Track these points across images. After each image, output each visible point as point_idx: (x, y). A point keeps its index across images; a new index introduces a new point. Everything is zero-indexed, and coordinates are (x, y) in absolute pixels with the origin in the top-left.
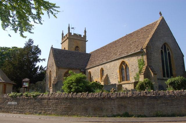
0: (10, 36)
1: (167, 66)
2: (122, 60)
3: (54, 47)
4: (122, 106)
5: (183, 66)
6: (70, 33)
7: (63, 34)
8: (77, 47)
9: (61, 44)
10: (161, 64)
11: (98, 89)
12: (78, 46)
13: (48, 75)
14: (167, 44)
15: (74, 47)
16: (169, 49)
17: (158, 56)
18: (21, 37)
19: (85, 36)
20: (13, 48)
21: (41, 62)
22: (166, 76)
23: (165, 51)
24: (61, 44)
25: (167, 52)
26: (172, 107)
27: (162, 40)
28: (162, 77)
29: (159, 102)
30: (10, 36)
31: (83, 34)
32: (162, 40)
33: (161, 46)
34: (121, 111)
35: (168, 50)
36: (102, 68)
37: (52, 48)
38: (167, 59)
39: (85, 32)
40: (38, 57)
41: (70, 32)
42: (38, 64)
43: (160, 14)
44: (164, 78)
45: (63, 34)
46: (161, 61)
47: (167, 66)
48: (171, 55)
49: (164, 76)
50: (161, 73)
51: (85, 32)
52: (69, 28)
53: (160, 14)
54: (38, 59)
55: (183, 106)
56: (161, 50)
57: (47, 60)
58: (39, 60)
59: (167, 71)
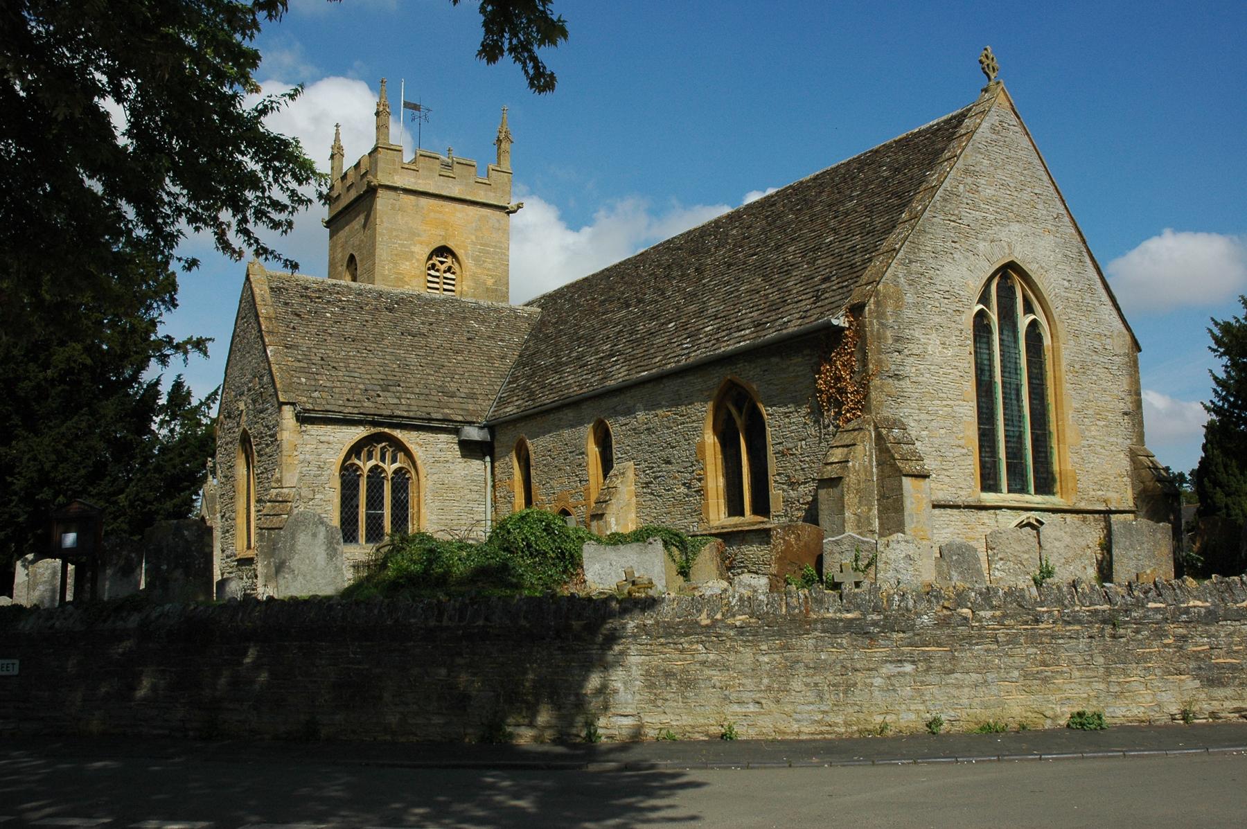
1: (1013, 420)
2: (727, 374)
4: (668, 674)
8: (443, 251)
10: (968, 410)
11: (116, 679)
13: (641, 801)
21: (176, 360)
22: (1032, 491)
23: (1008, 316)
25: (1024, 322)
27: (982, 246)
28: (971, 490)
29: (880, 652)
32: (982, 246)
33: (976, 285)
34: (659, 703)
35: (1029, 309)
38: (1017, 370)
40: (153, 324)
42: (209, 423)
44: (989, 498)
46: (970, 387)
47: (1013, 420)
48: (1047, 341)
49: (989, 482)
50: (972, 464)
54: (153, 337)
55: (1016, 673)
57: (219, 351)
58: (163, 349)
59: (1015, 454)
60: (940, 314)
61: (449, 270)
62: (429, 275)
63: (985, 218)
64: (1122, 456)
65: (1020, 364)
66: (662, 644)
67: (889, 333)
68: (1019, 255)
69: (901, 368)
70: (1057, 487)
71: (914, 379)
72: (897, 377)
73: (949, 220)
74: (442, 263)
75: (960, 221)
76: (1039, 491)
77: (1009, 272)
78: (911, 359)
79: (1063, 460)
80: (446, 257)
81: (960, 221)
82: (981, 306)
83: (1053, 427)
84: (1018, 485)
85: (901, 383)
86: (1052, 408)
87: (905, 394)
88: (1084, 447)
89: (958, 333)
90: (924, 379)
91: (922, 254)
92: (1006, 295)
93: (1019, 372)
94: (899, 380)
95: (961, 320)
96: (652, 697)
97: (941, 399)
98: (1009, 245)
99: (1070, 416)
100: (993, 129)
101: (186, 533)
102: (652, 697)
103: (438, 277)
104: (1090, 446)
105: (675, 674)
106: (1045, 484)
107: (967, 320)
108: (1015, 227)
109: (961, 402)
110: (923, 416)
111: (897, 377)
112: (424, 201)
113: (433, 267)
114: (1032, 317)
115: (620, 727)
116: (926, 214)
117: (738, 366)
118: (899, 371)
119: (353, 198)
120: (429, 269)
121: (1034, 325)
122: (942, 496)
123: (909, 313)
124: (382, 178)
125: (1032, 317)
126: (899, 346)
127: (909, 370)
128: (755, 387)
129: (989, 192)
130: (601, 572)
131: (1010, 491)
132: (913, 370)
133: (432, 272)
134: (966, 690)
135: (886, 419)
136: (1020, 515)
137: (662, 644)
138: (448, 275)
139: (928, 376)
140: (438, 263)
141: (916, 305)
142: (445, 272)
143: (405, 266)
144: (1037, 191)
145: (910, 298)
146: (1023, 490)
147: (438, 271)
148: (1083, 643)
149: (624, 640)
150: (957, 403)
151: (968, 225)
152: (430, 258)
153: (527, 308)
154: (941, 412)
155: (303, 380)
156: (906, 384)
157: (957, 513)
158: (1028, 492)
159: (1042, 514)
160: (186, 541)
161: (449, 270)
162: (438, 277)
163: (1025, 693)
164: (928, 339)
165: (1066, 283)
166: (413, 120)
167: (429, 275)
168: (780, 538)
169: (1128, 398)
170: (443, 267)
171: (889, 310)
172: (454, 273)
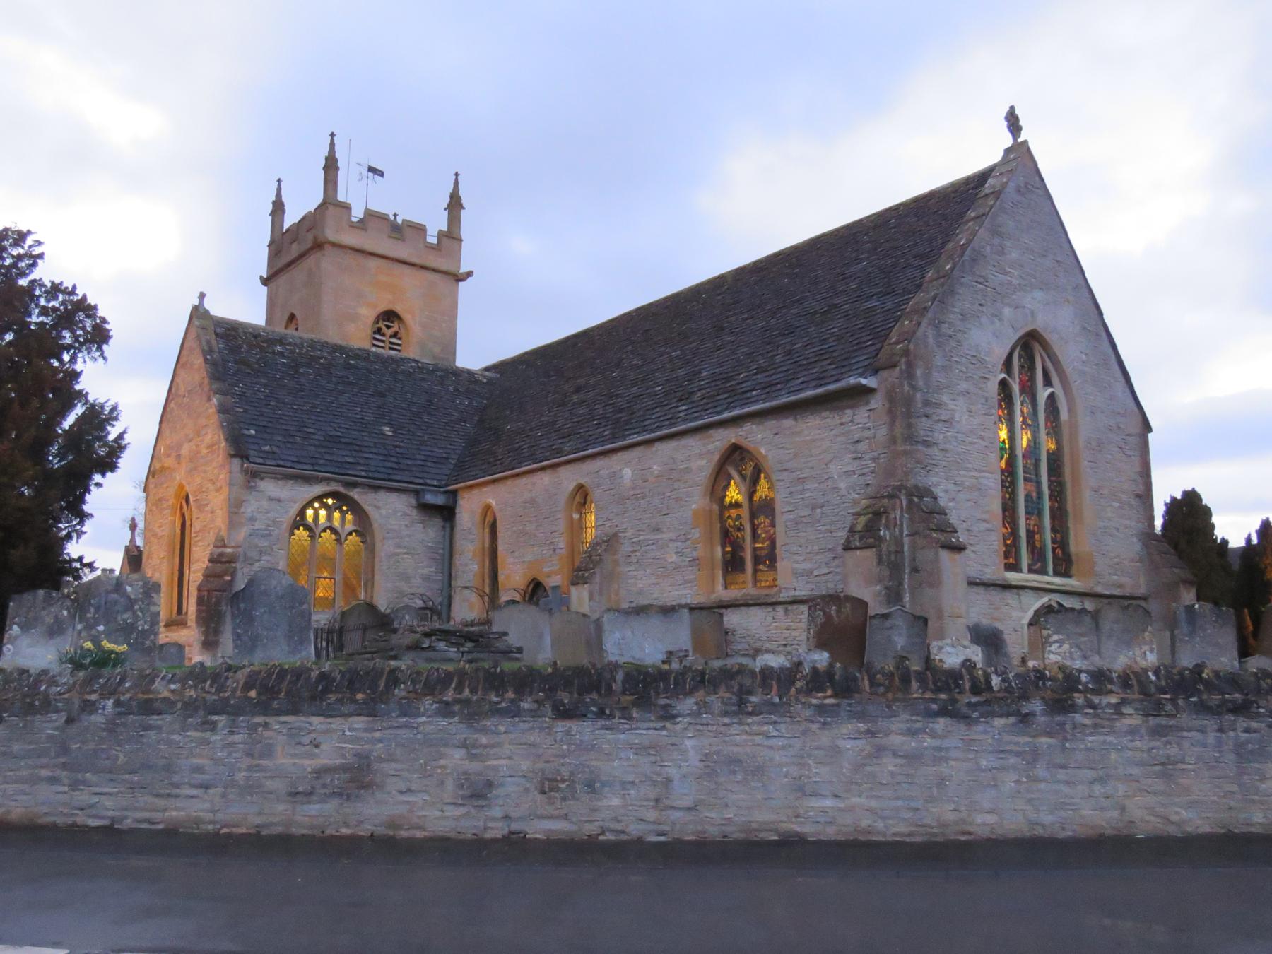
0: (381, 174)
3: (219, 308)
4: (734, 761)
5: (1139, 496)
6: (331, 203)
7: (278, 208)
8: (390, 316)
9: (265, 282)
12: (398, 308)
14: (1045, 345)
15: (368, 314)
16: (1055, 379)
17: (976, 421)
18: (464, 202)
19: (451, 236)
20: (1206, 506)
22: (1050, 569)
24: (265, 282)
25: (1043, 394)
26: (1062, 775)
28: (994, 570)
30: (381, 174)
31: (436, 223)
32: (1007, 311)
33: (1001, 352)
35: (1048, 382)
36: (580, 488)
37: (198, 313)
39: (455, 204)
41: (341, 197)
43: (1013, 123)
44: (1012, 577)
45: (278, 208)
48: (1064, 415)
51: (455, 204)
52: (331, 166)
53: (1013, 123)
56: (1004, 384)
60: (968, 378)
61: (395, 335)
62: (375, 339)
63: (1010, 283)
64: (1135, 540)
65: (1039, 437)
66: (725, 725)
67: (919, 396)
68: (1041, 322)
69: (930, 434)
70: (1074, 570)
71: (942, 446)
72: (927, 444)
73: (977, 282)
74: (388, 327)
75: (986, 284)
76: (1056, 573)
77: (1030, 343)
78: (940, 425)
79: (1079, 543)
80: (392, 322)
81: (986, 284)
82: (1003, 375)
83: (1069, 507)
84: (1038, 566)
85: (929, 450)
86: (1069, 486)
87: (933, 462)
88: (1100, 528)
89: (983, 401)
90: (952, 447)
91: (952, 316)
92: (1029, 365)
93: (1037, 446)
94: (928, 446)
95: (987, 387)
96: (713, 786)
97: (968, 470)
98: (1032, 313)
99: (1087, 495)
100: (1018, 190)
101: (129, 589)
102: (713, 786)
103: (383, 341)
104: (1105, 527)
105: (740, 761)
106: (1064, 565)
107: (993, 387)
108: (1038, 294)
109: (987, 475)
110: (951, 487)
111: (927, 444)
112: (373, 263)
113: (379, 331)
114: (1050, 390)
115: (674, 823)
116: (956, 273)
117: (745, 429)
118: (927, 436)
119: (294, 256)
120: (375, 333)
121: (1052, 397)
122: (974, 573)
123: (937, 376)
124: (330, 234)
125: (1050, 390)
126: (930, 411)
127: (938, 437)
128: (763, 451)
129: (1014, 255)
130: (621, 641)
131: (1031, 571)
132: (941, 437)
133: (378, 337)
134: (1080, 787)
135: (916, 487)
136: (1042, 597)
137: (725, 725)
138: (394, 340)
139: (955, 444)
140: (384, 328)
141: (944, 368)
142: (391, 337)
143: (351, 328)
144: (1059, 259)
145: (939, 361)
146: (1043, 571)
147: (383, 335)
148: (1211, 737)
149: (680, 719)
150: (983, 474)
151: (994, 289)
152: (377, 321)
153: (487, 373)
154: (967, 483)
155: (253, 432)
156: (934, 451)
157: (982, 592)
158: (1046, 573)
159: (1065, 597)
160: (129, 597)
161: (395, 335)
162: (383, 341)
163: (1146, 794)
164: (956, 405)
165: (1084, 357)
166: (361, 179)
167: (375, 339)
168: (820, 610)
169: (1139, 480)
170: (390, 332)
171: (919, 372)
172: (400, 339)
